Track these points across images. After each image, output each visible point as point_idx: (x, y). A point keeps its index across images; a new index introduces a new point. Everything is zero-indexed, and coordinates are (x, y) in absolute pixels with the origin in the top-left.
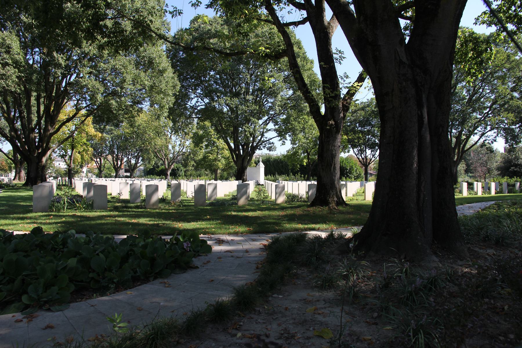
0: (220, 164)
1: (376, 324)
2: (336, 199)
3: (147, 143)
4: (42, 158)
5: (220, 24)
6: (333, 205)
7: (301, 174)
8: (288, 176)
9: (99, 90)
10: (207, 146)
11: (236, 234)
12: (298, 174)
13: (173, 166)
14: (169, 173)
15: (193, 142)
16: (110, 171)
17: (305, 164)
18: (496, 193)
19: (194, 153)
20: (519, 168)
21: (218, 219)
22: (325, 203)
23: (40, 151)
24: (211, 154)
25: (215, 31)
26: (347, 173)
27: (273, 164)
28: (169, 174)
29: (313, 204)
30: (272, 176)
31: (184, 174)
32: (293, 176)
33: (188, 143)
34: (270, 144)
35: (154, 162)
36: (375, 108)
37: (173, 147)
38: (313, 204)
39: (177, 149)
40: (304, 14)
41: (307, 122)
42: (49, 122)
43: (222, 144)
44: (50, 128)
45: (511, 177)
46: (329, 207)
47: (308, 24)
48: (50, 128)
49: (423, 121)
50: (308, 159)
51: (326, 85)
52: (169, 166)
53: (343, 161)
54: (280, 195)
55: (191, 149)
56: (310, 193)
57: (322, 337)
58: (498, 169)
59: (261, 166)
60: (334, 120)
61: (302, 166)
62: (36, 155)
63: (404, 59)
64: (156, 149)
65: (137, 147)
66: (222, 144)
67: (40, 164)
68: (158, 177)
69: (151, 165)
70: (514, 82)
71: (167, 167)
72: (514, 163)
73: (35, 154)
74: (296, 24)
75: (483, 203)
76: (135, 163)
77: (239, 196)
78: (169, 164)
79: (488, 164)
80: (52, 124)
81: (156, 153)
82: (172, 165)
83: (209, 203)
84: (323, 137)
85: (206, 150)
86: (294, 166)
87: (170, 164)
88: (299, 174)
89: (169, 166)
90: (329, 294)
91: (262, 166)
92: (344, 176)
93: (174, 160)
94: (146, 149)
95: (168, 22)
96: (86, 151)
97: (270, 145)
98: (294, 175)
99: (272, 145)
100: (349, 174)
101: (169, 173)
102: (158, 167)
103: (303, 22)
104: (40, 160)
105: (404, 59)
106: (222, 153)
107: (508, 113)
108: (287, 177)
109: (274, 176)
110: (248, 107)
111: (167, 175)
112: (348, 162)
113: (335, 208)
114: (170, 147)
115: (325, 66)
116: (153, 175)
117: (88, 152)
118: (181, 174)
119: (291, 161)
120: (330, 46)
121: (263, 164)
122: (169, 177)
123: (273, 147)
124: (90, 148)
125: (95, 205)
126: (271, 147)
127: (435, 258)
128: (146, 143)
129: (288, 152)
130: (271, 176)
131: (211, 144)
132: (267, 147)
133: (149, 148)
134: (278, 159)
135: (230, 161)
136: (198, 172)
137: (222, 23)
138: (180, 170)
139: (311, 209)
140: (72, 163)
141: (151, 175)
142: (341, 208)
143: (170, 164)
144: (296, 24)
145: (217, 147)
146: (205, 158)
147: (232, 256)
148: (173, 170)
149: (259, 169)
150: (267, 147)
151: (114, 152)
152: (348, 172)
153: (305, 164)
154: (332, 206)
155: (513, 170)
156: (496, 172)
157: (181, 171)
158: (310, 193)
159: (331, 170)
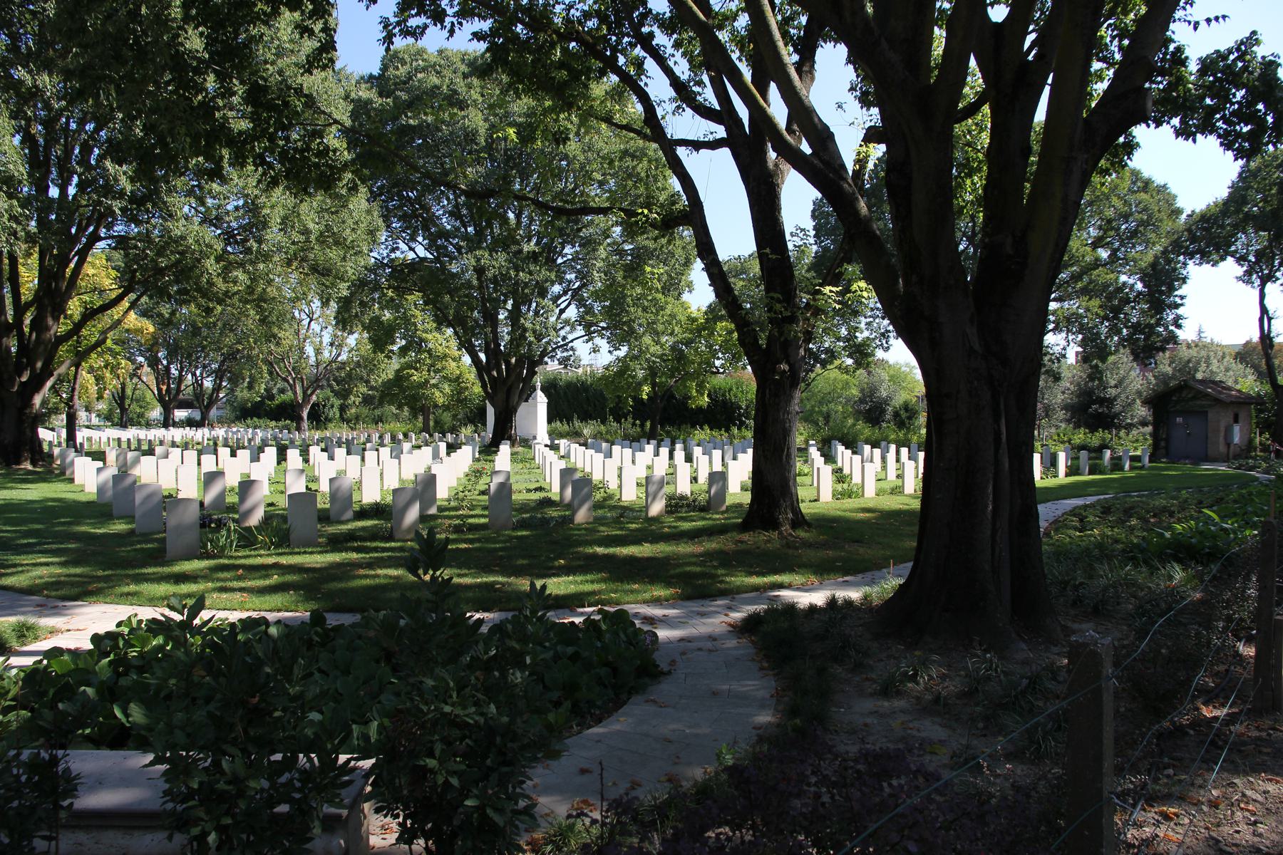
0: (437, 394)
1: (985, 736)
2: (790, 515)
3: (251, 340)
4: (31, 397)
5: (460, 74)
6: (786, 528)
7: (635, 419)
8: (603, 422)
9: (211, 248)
10: (404, 351)
11: (657, 601)
12: (626, 420)
13: (314, 398)
14: (305, 415)
15: (371, 340)
16: (141, 407)
17: (645, 397)
18: (1067, 475)
19: (368, 365)
20: (1108, 407)
21: (600, 571)
22: (773, 524)
23: (24, 379)
24: (416, 369)
25: (451, 90)
26: (740, 415)
27: (565, 393)
28: (305, 417)
29: (746, 526)
30: (565, 422)
31: (338, 415)
32: (615, 424)
33: (352, 340)
34: (567, 350)
35: (263, 386)
36: (808, 271)
37: (318, 352)
38: (746, 526)
39: (326, 354)
40: (720, 132)
41: (663, 309)
42: (49, 309)
43: (441, 345)
44: (50, 321)
45: (1093, 430)
46: (781, 533)
47: (725, 153)
48: (50, 321)
49: (1001, 439)
50: (654, 385)
51: (772, 294)
52: (306, 397)
53: (731, 390)
54: (654, 499)
55: (362, 357)
56: (713, 492)
57: (936, 754)
58: (1066, 407)
59: (539, 399)
60: (788, 363)
61: (638, 400)
62: (16, 388)
63: (977, 347)
64: (272, 354)
65: (225, 350)
66: (441, 345)
67: (27, 411)
68: (273, 423)
69: (257, 393)
70: (1100, 228)
71: (300, 399)
72: (1098, 397)
73: (13, 388)
74: (697, 145)
75: (1049, 504)
76: (214, 389)
77: (576, 503)
78: (304, 393)
79: (1046, 396)
80: (57, 314)
81: (271, 364)
82: (312, 393)
83: (518, 521)
84: (768, 396)
85: (403, 360)
86: (620, 401)
87: (309, 392)
88: (630, 419)
89: (306, 397)
90: (899, 703)
91: (541, 400)
92: (735, 425)
93: (316, 383)
94: (249, 357)
95: (348, 72)
96: (112, 368)
97: (565, 354)
98: (619, 422)
99: (571, 353)
100: (746, 418)
101: (305, 415)
102: (271, 397)
103: (714, 145)
104: (28, 402)
105: (977, 347)
106: (443, 369)
107: (1090, 299)
108: (602, 427)
109: (568, 424)
110: (531, 273)
111: (302, 419)
112: (742, 392)
113: (791, 535)
114: (309, 350)
115: (774, 257)
116: (259, 417)
117: (119, 371)
118: (331, 414)
119: (614, 390)
120: (779, 213)
121: (543, 395)
122: (305, 424)
123: (572, 359)
124: (123, 362)
125: (292, 537)
126: (568, 358)
127: (1024, 646)
128: (248, 342)
129: (607, 369)
130: (561, 422)
131: (414, 344)
132: (558, 357)
133: (255, 352)
134: (578, 381)
135: (462, 388)
136: (377, 412)
137: (466, 70)
138: (328, 406)
139: (746, 537)
140: (76, 397)
141: (255, 419)
142: (802, 534)
143: (309, 392)
144: (697, 145)
145: (429, 351)
146: (400, 378)
147: (700, 649)
148: (315, 405)
149: (536, 406)
150: (558, 357)
151: (158, 361)
152: (743, 415)
153: (645, 397)
154: (786, 530)
155: (1096, 410)
156: (1061, 414)
157: (332, 406)
158: (713, 492)
159: (781, 459)
